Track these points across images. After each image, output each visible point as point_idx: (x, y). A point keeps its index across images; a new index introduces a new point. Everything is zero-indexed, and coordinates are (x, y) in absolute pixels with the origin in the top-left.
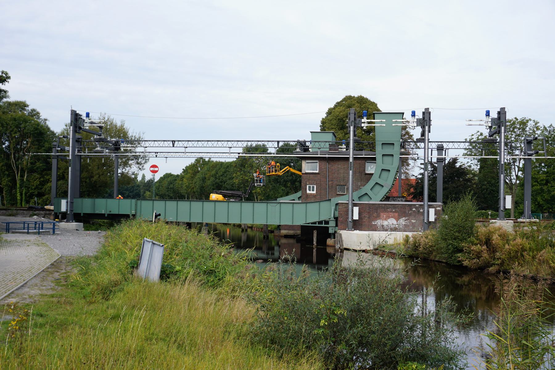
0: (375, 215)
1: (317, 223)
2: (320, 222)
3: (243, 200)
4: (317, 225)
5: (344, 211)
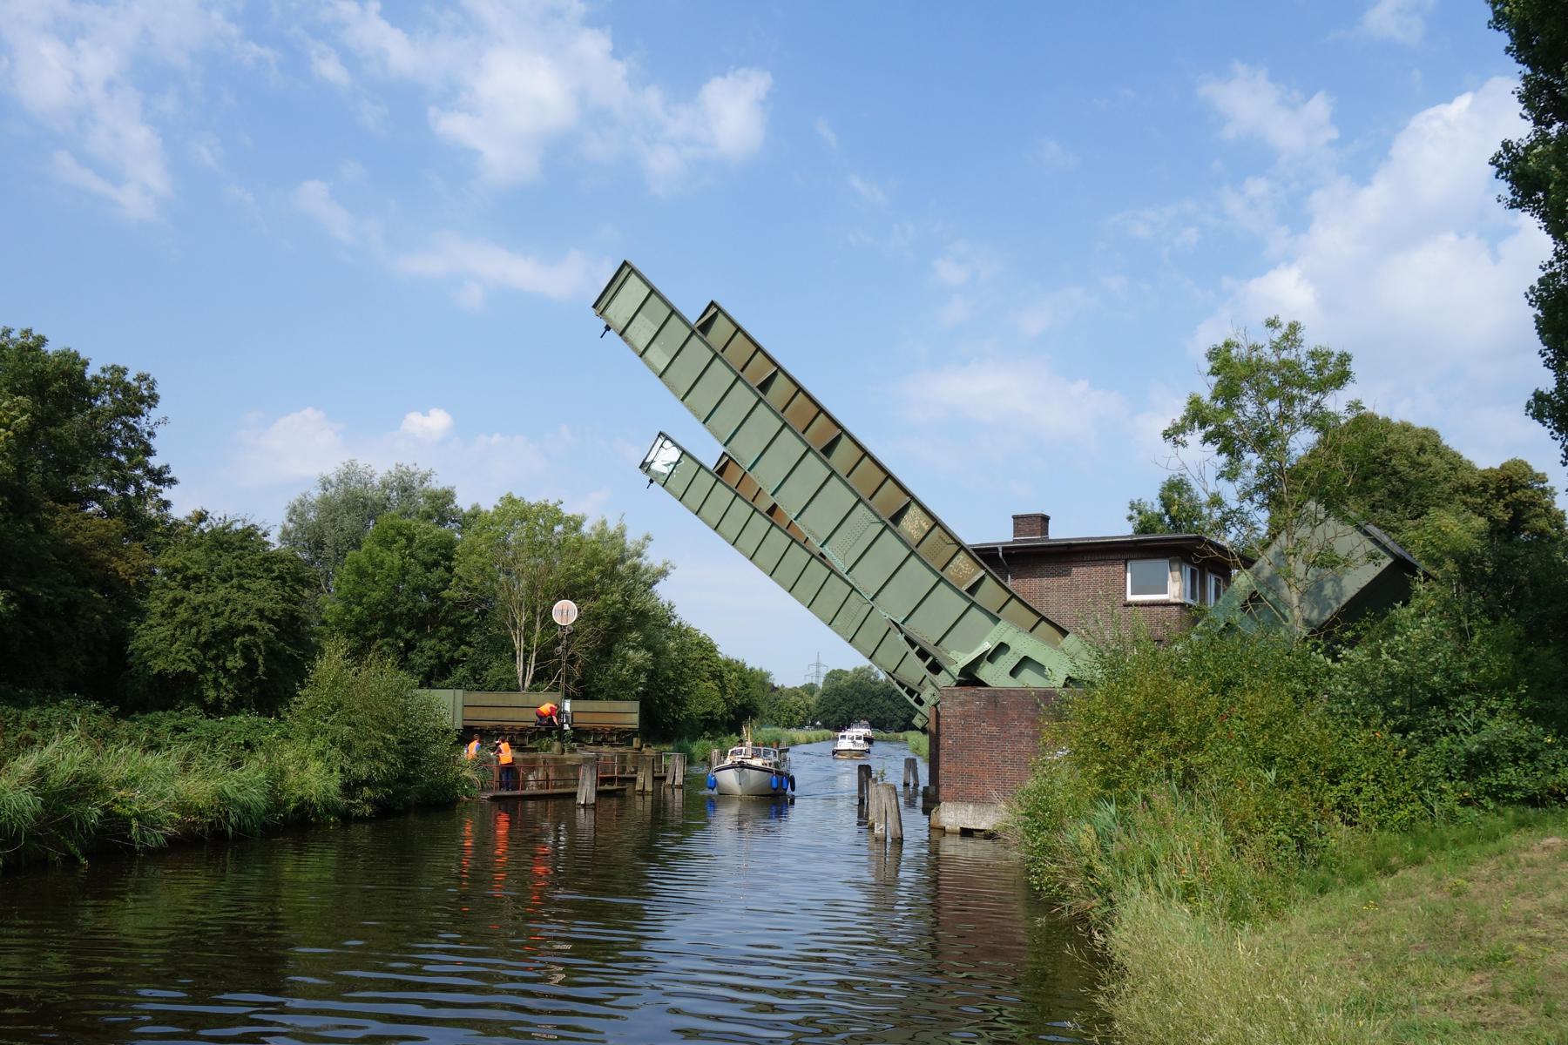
1: (917, 648)
2: (911, 692)
3: (1000, 550)
4: (903, 692)
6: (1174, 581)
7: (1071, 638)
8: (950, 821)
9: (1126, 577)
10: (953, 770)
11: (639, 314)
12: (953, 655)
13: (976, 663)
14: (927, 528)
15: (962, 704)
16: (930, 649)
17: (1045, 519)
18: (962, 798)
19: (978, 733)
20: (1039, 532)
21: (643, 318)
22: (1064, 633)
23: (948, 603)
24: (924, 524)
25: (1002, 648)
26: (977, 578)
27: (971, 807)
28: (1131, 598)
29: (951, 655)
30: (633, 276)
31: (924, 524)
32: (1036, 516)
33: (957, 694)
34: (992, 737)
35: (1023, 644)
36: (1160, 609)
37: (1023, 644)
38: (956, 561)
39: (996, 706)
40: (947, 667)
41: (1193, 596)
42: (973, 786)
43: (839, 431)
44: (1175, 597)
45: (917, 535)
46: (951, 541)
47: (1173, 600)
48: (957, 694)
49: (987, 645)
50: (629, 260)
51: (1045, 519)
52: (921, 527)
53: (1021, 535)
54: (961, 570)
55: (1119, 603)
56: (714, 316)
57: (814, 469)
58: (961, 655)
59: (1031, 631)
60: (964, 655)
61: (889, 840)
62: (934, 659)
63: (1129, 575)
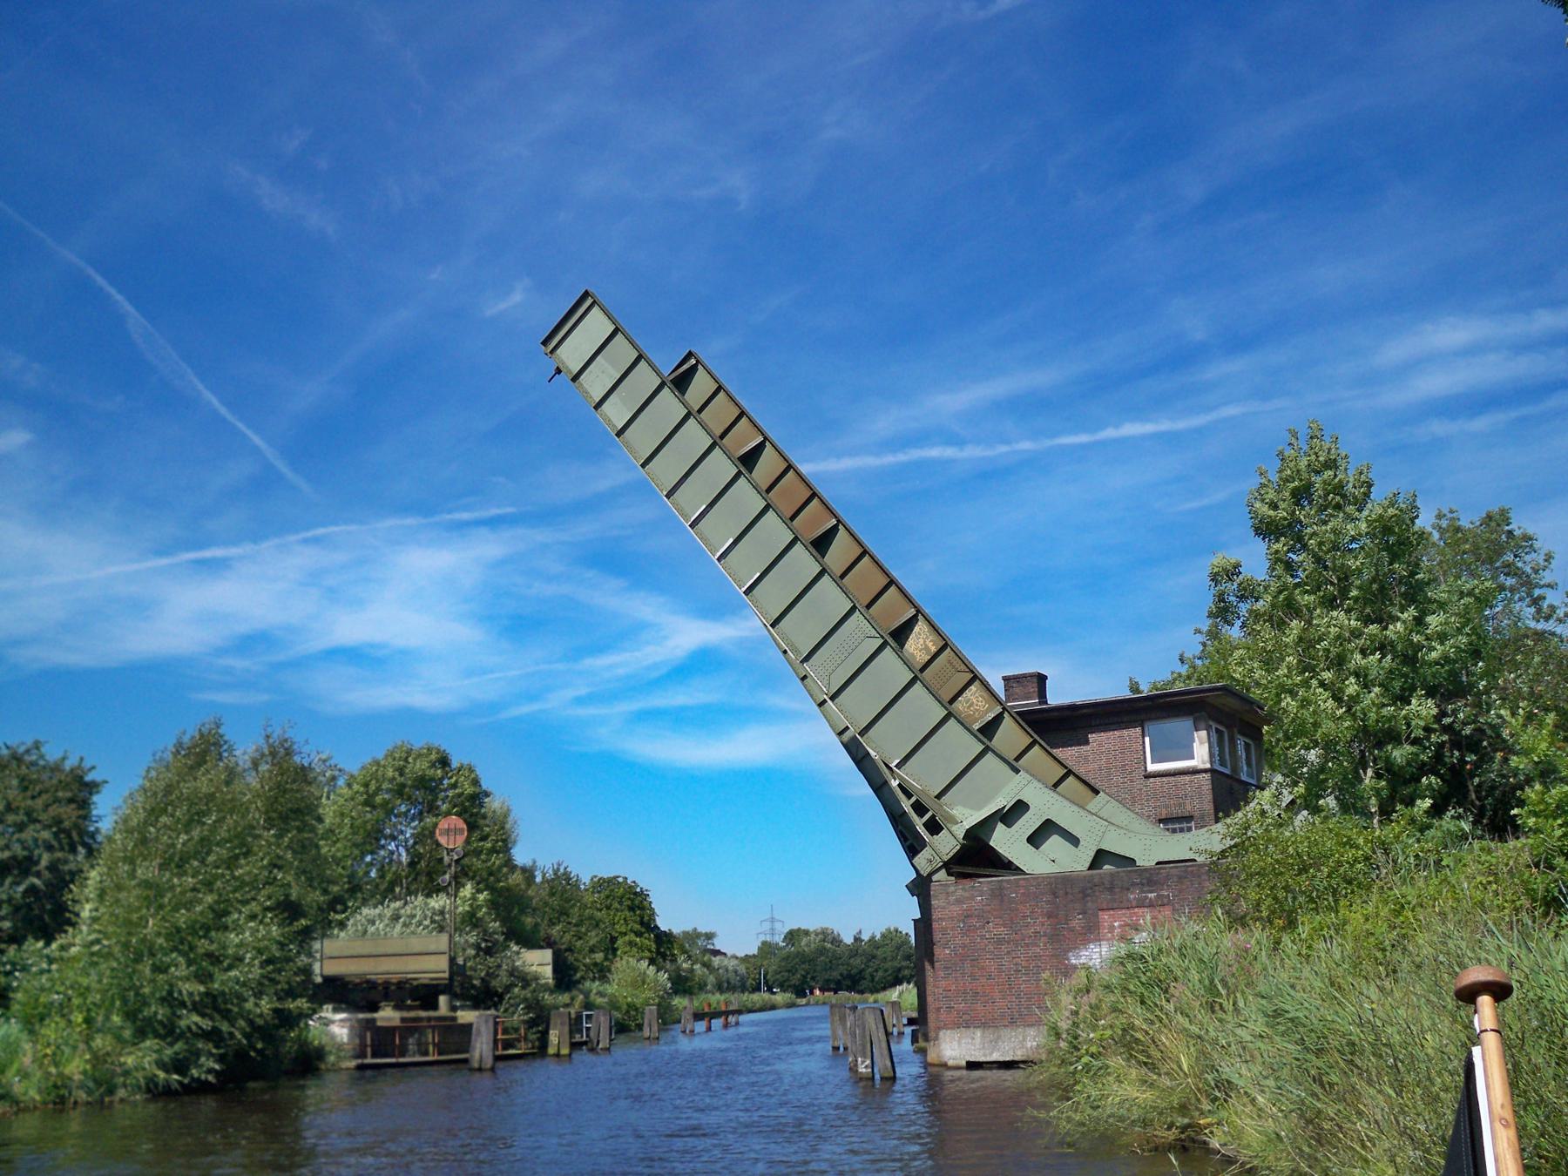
0: (1077, 922)
1: (914, 799)
5: (952, 918)
6: (1201, 743)
7: (1102, 794)
8: (954, 1053)
9: (1144, 742)
10: (953, 988)
11: (599, 358)
12: (957, 812)
13: (987, 824)
14: (934, 649)
15: (959, 902)
16: (926, 802)
17: (1042, 679)
18: (966, 1022)
19: (983, 937)
20: (1036, 694)
21: (603, 362)
22: (1096, 792)
23: (958, 744)
24: (930, 645)
25: (1020, 807)
26: (990, 716)
27: (979, 1033)
28: (1152, 767)
29: (954, 812)
30: (596, 310)
31: (930, 645)
32: (1031, 675)
33: (952, 889)
34: (1000, 942)
35: (1044, 804)
36: (1187, 778)
37: (1044, 804)
38: (967, 694)
39: (1002, 901)
40: (949, 825)
41: (1223, 763)
42: (979, 1007)
43: (834, 522)
44: (1204, 763)
45: (921, 658)
46: (963, 667)
47: (1202, 766)
48: (952, 889)
49: (1003, 801)
50: (591, 290)
51: (1042, 679)
52: (927, 648)
53: (1014, 700)
54: (972, 705)
55: (1139, 773)
56: (693, 369)
57: (802, 562)
58: (967, 811)
59: (1056, 785)
60: (972, 812)
61: (877, 1077)
62: (933, 817)
63: (1147, 739)
